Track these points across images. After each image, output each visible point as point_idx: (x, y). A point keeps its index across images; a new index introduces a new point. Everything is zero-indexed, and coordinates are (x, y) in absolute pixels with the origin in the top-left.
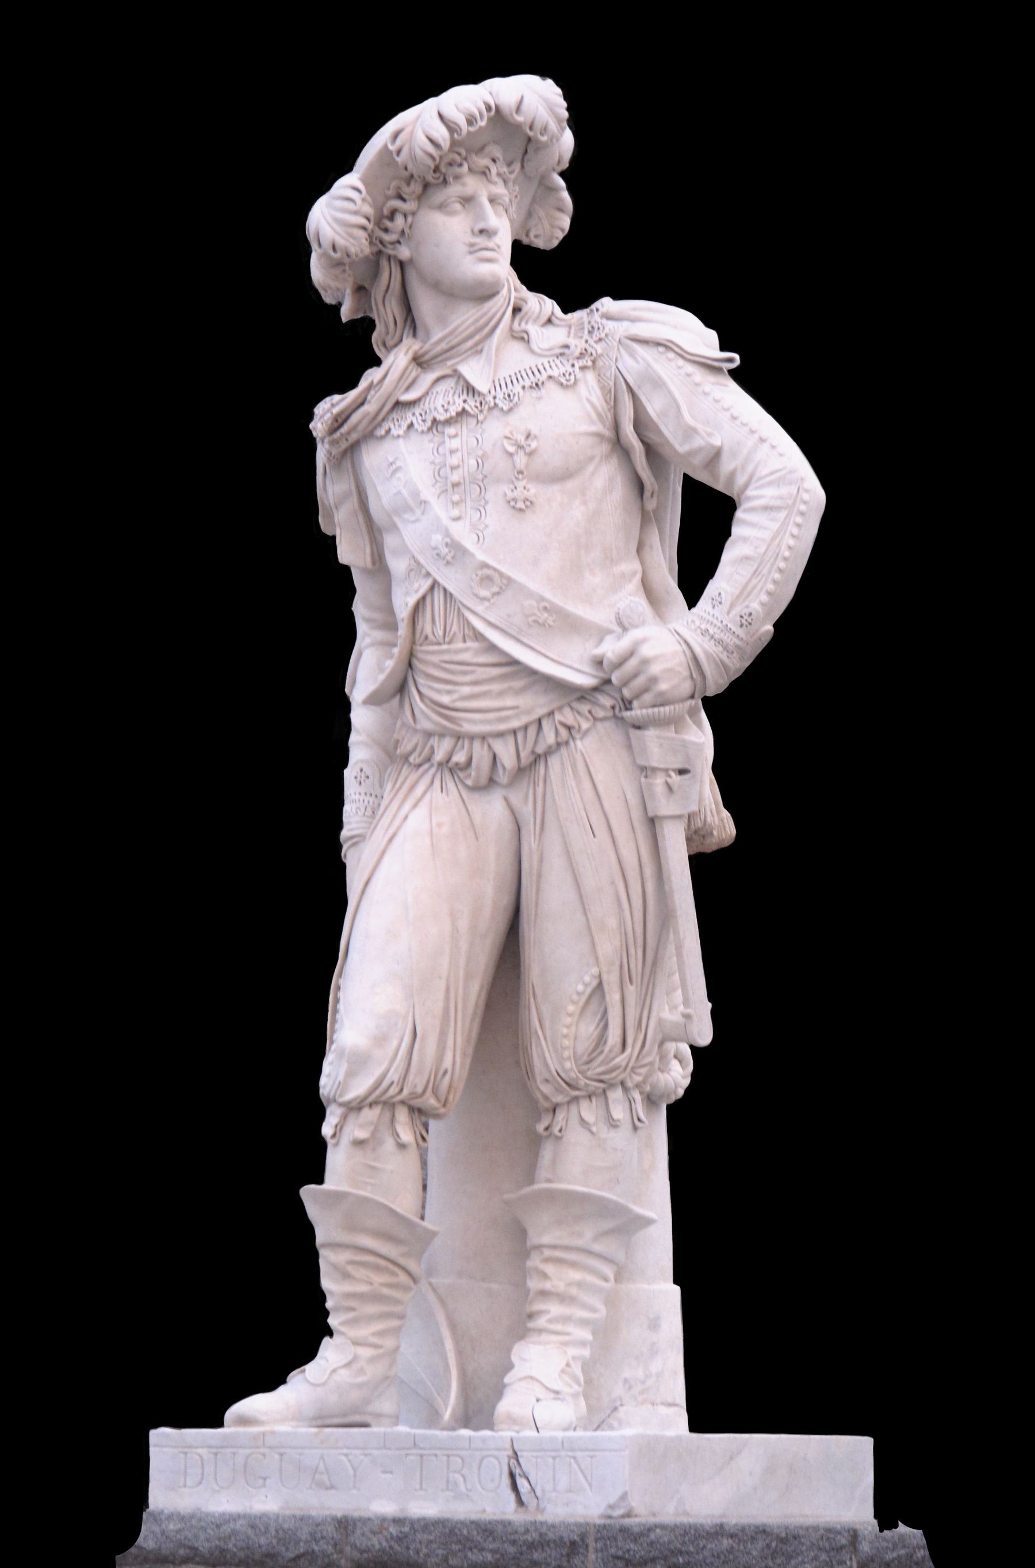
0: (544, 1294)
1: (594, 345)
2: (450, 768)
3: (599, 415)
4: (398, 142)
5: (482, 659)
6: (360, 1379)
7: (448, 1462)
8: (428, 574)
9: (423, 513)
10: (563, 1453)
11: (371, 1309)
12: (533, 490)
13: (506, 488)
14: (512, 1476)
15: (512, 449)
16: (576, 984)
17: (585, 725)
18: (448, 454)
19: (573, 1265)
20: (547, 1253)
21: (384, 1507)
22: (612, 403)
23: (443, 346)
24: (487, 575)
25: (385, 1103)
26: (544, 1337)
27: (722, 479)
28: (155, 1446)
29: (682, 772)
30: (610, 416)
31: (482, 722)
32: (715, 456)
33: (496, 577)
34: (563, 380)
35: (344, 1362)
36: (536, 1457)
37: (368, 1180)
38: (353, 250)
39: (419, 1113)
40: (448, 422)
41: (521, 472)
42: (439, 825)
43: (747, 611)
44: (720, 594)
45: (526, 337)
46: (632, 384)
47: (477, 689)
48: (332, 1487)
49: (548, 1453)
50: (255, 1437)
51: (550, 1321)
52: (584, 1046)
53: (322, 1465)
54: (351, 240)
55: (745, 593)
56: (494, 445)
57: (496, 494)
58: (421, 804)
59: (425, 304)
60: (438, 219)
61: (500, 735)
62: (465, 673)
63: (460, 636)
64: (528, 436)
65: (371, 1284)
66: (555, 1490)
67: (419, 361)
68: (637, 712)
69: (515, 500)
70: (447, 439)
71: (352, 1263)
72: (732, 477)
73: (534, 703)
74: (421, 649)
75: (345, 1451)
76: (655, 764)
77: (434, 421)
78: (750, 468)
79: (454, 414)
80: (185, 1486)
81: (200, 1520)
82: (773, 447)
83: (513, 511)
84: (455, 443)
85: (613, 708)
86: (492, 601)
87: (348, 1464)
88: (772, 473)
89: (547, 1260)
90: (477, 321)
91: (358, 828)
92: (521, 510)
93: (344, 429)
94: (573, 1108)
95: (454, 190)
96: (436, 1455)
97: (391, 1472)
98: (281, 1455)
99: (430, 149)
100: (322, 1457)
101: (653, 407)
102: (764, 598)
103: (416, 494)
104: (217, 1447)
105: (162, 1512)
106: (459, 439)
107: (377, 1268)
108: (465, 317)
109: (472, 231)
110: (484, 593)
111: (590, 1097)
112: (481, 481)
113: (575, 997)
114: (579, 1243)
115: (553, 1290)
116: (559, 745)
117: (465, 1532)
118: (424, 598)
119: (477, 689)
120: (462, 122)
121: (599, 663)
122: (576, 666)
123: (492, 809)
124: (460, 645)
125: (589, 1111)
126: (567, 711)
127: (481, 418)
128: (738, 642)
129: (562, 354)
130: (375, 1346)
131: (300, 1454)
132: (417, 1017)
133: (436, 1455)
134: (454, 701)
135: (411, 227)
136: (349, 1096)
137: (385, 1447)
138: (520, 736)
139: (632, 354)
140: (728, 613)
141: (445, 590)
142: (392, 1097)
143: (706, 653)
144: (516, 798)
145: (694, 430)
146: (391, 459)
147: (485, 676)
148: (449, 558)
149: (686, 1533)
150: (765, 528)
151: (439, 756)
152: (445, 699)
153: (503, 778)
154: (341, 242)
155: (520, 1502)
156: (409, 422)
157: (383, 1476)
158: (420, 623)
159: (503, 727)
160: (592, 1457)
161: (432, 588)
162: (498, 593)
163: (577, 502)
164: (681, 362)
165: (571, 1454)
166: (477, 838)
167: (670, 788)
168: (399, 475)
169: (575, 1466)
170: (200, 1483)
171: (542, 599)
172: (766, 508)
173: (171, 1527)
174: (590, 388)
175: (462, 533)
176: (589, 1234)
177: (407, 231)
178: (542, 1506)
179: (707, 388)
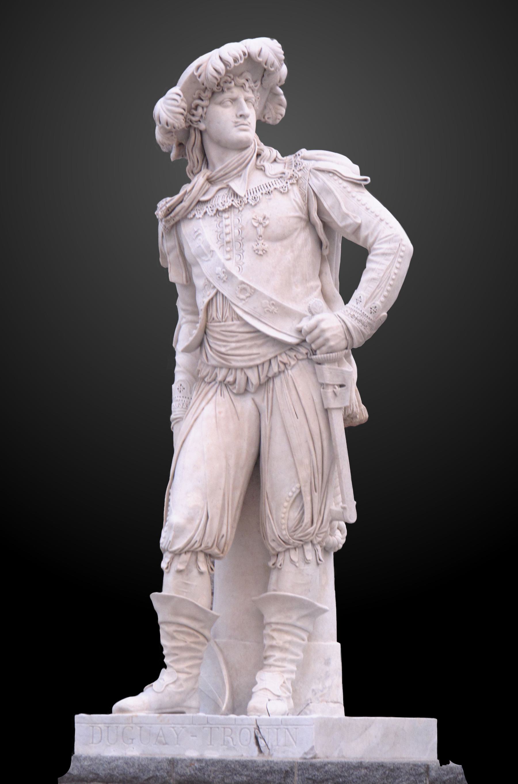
0: (272, 647)
1: (298, 173)
2: (225, 384)
3: (300, 208)
4: (199, 71)
5: (241, 330)
6: (180, 690)
7: (224, 731)
8: (214, 287)
9: (212, 257)
10: (282, 727)
11: (186, 654)
12: (267, 245)
13: (253, 244)
14: (256, 738)
15: (256, 225)
16: (289, 492)
17: (293, 363)
18: (224, 227)
19: (287, 632)
20: (274, 626)
21: (192, 753)
22: (306, 202)
23: (222, 173)
24: (244, 288)
25: (193, 552)
26: (272, 669)
27: (362, 239)
28: (78, 723)
29: (341, 386)
30: (305, 208)
31: (241, 361)
32: (358, 228)
33: (248, 289)
34: (282, 190)
35: (172, 681)
36: (268, 729)
37: (184, 590)
38: (177, 125)
39: (210, 557)
40: (224, 211)
41: (261, 236)
42: (220, 413)
43: (374, 305)
44: (360, 297)
45: (263, 168)
46: (316, 192)
47: (239, 345)
48: (166, 744)
49: (274, 727)
50: (128, 718)
51: (275, 661)
52: (292, 523)
53: (161, 733)
54: (176, 120)
55: (373, 297)
56: (247, 222)
57: (248, 247)
58: (210, 402)
59: (213, 152)
60: (219, 109)
61: (250, 367)
62: (233, 337)
63: (230, 318)
64: (264, 218)
65: (186, 642)
66: (278, 745)
67: (210, 181)
68: (319, 356)
69: (258, 250)
70: (224, 220)
71: (176, 631)
72: (366, 238)
73: (267, 352)
74: (211, 325)
75: (173, 725)
76: (328, 382)
77: (217, 210)
78: (375, 234)
79: (227, 207)
80: (92, 743)
81: (100, 760)
82: (387, 224)
83: (257, 256)
84: (228, 222)
85: (307, 354)
86: (246, 300)
87: (174, 732)
88: (386, 237)
89: (274, 630)
90: (239, 160)
91: (179, 414)
92: (261, 255)
93: (172, 215)
94: (287, 554)
95: (227, 95)
96: (218, 728)
97: (196, 736)
98: (141, 727)
99: (215, 74)
100: (161, 729)
101: (327, 204)
102: (382, 299)
103: (208, 247)
104: (109, 724)
105: (81, 756)
106: (230, 219)
107: (189, 634)
108: (233, 159)
109: (236, 115)
110: (242, 296)
111: (295, 548)
112: (241, 241)
113: (288, 499)
114: (290, 621)
115: (277, 645)
116: (280, 372)
117: (233, 766)
118: (212, 299)
119: (239, 345)
120: (231, 61)
121: (300, 331)
122: (288, 333)
123: (246, 405)
124: (230, 323)
125: (295, 556)
126: (284, 356)
127: (241, 209)
128: (369, 321)
129: (281, 177)
130: (188, 673)
131: (150, 727)
132: (209, 508)
133: (218, 728)
134: (227, 351)
135: (205, 113)
136: (175, 548)
137: (192, 724)
138: (260, 368)
139: (316, 177)
140: (365, 306)
141: (223, 295)
142: (196, 548)
143: (354, 327)
144: (258, 399)
145: (348, 215)
146: (196, 230)
147: (243, 338)
148: (225, 279)
149: (343, 766)
150: (383, 264)
151: (220, 378)
152: (223, 350)
153: (252, 389)
154: (170, 121)
155: (260, 751)
156: (204, 211)
157: (192, 738)
158: (210, 312)
159: (252, 363)
160: (296, 729)
161: (216, 294)
162: (249, 297)
163: (289, 251)
164: (341, 181)
165: (286, 727)
166: (239, 419)
167: (335, 394)
168: (200, 237)
169: (288, 733)
170: (100, 741)
171: (271, 299)
172: (384, 254)
173: (86, 763)
174: (295, 194)
175: (231, 266)
176: (295, 617)
177: (204, 115)
178: (271, 753)
179: (354, 194)
